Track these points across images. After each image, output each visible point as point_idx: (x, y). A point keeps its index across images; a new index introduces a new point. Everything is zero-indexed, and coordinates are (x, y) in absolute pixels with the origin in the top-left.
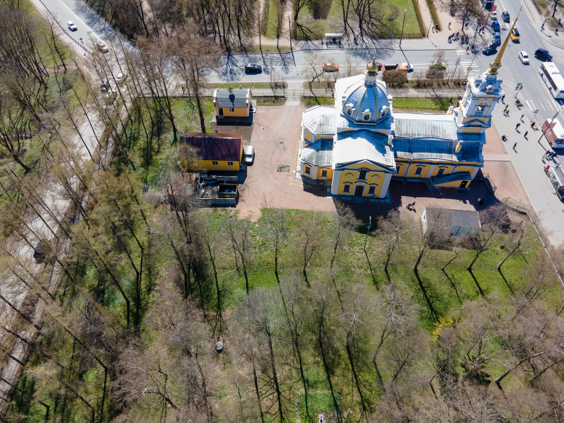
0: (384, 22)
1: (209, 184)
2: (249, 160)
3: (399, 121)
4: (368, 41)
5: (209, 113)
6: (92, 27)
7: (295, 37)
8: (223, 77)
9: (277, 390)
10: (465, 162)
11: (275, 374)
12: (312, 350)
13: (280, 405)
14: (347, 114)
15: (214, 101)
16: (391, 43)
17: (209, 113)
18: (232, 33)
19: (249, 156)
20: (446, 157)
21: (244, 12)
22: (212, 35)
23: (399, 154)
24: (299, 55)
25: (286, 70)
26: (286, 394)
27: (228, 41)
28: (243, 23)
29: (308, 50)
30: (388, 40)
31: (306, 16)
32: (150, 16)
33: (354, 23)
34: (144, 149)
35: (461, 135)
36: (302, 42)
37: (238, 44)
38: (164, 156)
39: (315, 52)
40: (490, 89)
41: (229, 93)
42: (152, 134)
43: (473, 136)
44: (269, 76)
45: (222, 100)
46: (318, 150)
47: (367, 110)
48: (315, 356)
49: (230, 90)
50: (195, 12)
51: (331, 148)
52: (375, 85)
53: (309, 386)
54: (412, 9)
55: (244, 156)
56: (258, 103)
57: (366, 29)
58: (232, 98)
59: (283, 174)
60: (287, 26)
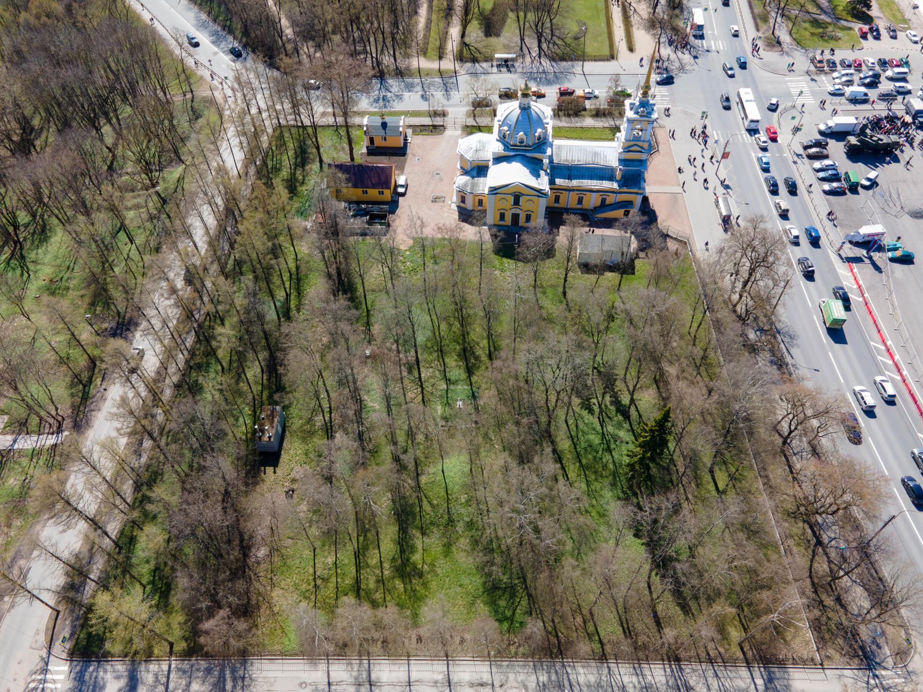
0: (569, 41)
1: (359, 214)
2: (401, 190)
3: (559, 147)
4: (546, 63)
5: (359, 144)
6: (218, 46)
7: (460, 58)
8: (375, 105)
9: (422, 386)
10: (625, 189)
11: (420, 374)
12: (456, 357)
13: (423, 397)
14: (503, 138)
15: (365, 129)
16: (573, 66)
17: (359, 144)
18: (386, 53)
19: (402, 186)
20: (606, 185)
21: (401, 28)
22: (362, 56)
23: (558, 181)
24: (463, 79)
25: (448, 96)
26: (429, 389)
27: (381, 63)
28: (400, 42)
29: (475, 74)
30: (570, 63)
31: (475, 32)
32: (289, 32)
33: (532, 42)
34: (287, 181)
35: (622, 161)
36: (469, 65)
37: (393, 67)
38: (310, 187)
39: (483, 77)
40: (643, 112)
41: (381, 121)
42: (296, 165)
43: (635, 163)
44: (426, 103)
45: (375, 128)
46: (473, 177)
47: (521, 133)
48: (456, 361)
49: (382, 116)
50: (343, 29)
51: (485, 176)
52: (529, 107)
53: (451, 383)
54: (604, 25)
55: (396, 186)
56: (414, 132)
57: (546, 49)
58: (384, 125)
59: (438, 205)
60: (453, 45)
